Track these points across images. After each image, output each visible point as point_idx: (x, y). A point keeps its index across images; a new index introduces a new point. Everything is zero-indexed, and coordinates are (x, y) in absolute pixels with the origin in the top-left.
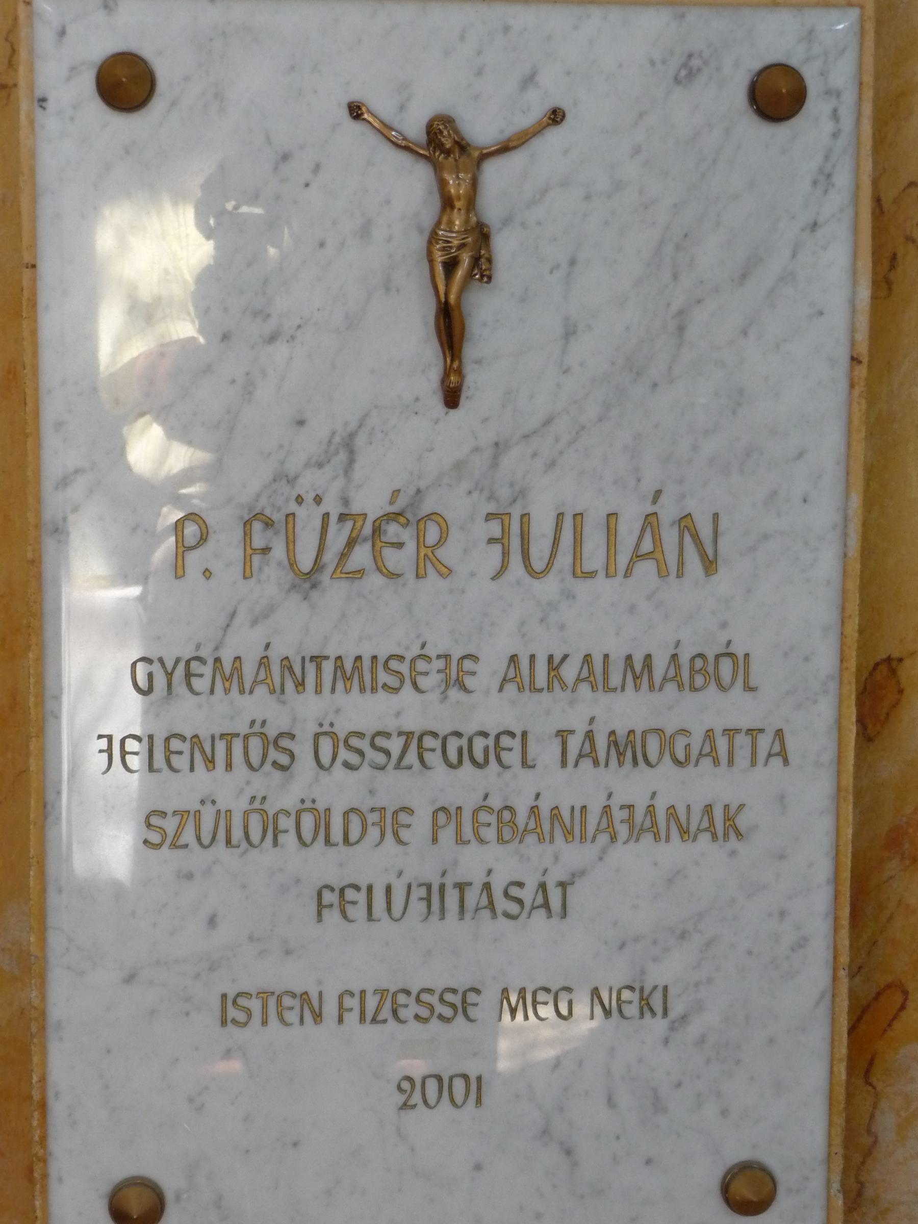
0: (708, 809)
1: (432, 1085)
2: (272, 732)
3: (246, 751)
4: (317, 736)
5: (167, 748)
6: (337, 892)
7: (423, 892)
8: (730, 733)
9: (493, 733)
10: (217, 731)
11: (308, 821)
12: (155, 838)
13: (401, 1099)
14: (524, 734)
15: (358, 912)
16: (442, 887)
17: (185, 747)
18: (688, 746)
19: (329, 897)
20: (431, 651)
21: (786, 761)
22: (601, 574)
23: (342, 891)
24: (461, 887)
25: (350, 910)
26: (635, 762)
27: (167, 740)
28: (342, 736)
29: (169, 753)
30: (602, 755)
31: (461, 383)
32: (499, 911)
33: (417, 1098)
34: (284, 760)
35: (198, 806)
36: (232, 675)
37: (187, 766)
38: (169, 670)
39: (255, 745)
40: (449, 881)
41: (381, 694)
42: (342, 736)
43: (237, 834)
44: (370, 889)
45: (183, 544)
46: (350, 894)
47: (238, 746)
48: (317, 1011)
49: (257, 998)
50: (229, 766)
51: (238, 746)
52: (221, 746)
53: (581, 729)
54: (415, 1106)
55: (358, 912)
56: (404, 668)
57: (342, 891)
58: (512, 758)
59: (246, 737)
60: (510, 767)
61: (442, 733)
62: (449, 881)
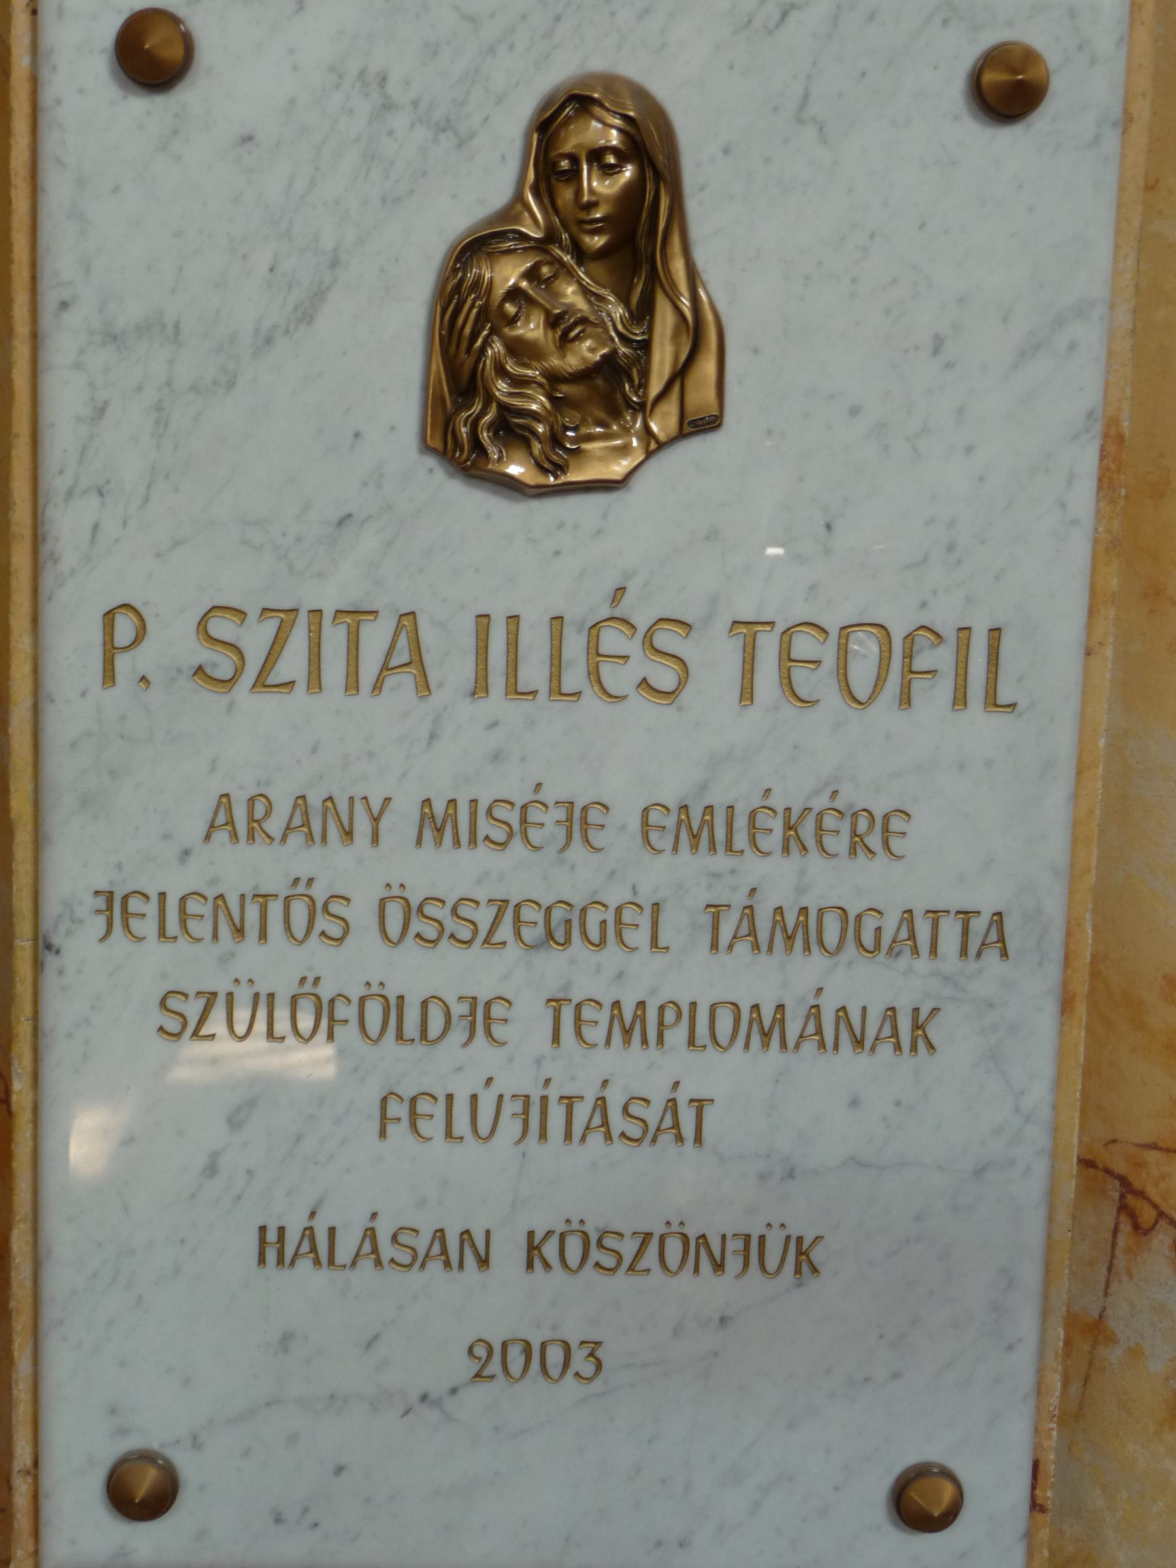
0: (891, 1012)
1: (515, 1353)
2: (319, 893)
3: (582, 922)
4: (383, 903)
5: (182, 909)
6: (406, 1105)
7: (518, 1107)
8: (935, 915)
9: (613, 905)
10: (247, 889)
11: (374, 1012)
12: (173, 1025)
13: (475, 1367)
14: (656, 906)
15: (433, 1128)
16: (544, 1099)
17: (206, 910)
18: (879, 929)
19: (396, 1109)
20: (547, 795)
21: (1004, 954)
22: (301, 686)
23: (413, 1100)
24: (569, 1102)
25: (423, 1126)
26: (807, 948)
27: (183, 900)
28: (415, 903)
29: (183, 915)
30: (763, 936)
31: (516, 433)
32: (615, 1133)
33: (495, 1367)
34: (335, 930)
35: (232, 988)
36: (444, 822)
37: (208, 935)
38: (376, 813)
39: (299, 911)
40: (553, 1093)
41: (482, 848)
42: (415, 903)
43: (411, 1027)
44: (450, 1098)
45: (597, 649)
46: (423, 1106)
47: (275, 910)
48: (718, 1259)
49: (631, 1238)
50: (263, 935)
51: (275, 910)
52: (253, 912)
53: (739, 899)
54: (492, 1377)
55: (433, 1128)
56: (514, 818)
57: (413, 1100)
58: (640, 937)
59: (288, 900)
60: (145, 938)
61: (546, 902)
62: (553, 1093)
